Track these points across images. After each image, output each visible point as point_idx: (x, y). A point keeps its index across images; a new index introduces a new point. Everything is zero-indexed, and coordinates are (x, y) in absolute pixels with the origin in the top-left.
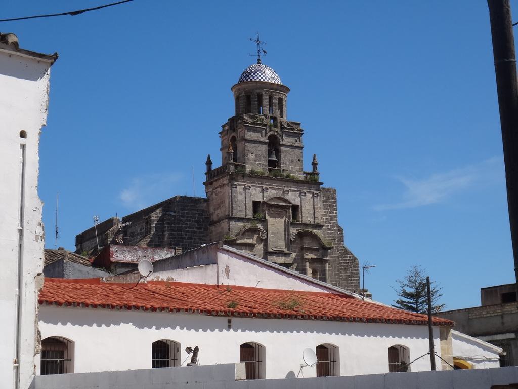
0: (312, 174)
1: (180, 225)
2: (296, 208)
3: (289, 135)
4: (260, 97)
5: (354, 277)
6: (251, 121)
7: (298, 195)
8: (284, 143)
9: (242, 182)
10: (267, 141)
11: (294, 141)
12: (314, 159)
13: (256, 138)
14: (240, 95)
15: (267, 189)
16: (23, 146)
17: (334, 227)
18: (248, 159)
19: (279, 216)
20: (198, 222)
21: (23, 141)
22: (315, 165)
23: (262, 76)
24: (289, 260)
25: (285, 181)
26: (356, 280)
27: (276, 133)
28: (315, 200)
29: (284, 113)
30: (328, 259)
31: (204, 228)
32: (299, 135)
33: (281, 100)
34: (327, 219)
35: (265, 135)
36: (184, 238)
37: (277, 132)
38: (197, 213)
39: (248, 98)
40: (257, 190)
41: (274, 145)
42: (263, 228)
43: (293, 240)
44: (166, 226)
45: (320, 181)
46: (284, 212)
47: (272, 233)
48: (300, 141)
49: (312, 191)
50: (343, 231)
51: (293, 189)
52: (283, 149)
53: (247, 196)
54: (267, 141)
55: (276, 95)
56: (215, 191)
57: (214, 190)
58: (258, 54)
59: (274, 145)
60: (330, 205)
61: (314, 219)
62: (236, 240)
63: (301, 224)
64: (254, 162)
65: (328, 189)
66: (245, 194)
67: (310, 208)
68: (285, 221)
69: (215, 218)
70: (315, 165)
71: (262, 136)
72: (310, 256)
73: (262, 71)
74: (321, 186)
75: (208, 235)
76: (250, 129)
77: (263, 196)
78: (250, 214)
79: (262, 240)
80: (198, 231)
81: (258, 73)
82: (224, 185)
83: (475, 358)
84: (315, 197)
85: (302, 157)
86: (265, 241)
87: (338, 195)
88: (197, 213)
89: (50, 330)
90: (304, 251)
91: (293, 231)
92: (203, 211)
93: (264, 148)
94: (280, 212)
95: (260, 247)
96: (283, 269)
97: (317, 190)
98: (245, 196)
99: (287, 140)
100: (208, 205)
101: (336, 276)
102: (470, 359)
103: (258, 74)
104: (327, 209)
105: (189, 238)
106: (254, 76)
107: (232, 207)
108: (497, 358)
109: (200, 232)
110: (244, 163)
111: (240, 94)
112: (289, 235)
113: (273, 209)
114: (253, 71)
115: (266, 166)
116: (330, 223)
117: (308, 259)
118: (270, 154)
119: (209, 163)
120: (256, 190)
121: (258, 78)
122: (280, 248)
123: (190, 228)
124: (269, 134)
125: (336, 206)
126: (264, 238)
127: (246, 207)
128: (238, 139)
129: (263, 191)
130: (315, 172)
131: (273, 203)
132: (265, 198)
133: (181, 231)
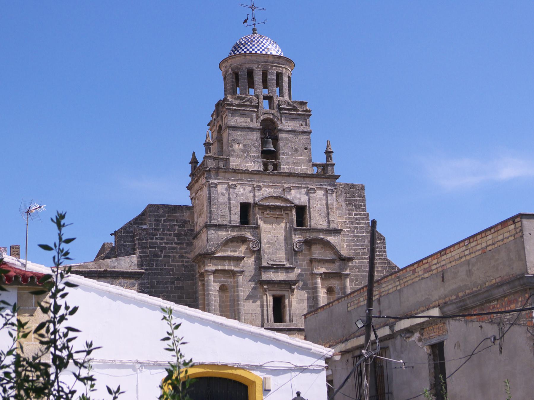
0: (325, 167)
1: (154, 241)
2: (302, 211)
3: (291, 118)
4: (250, 74)
6: (236, 102)
7: (304, 192)
8: (284, 128)
9: (225, 180)
10: (259, 126)
11: (298, 125)
12: (328, 146)
13: (244, 124)
15: (259, 187)
17: (363, 232)
18: (233, 151)
19: (277, 220)
20: (178, 235)
22: (328, 153)
23: (253, 48)
24: (292, 276)
25: (284, 176)
27: (271, 117)
28: (329, 198)
29: (284, 91)
30: (348, 272)
32: (306, 116)
33: (279, 76)
34: (352, 223)
35: (257, 119)
36: (160, 256)
37: (273, 114)
38: (176, 225)
40: (246, 190)
41: (269, 131)
42: (253, 236)
43: (296, 249)
44: (137, 242)
45: (336, 173)
46: (285, 215)
48: (306, 125)
49: (324, 187)
50: (384, 239)
51: (297, 185)
52: (282, 135)
53: (231, 197)
54: (259, 126)
55: (272, 69)
57: (196, 194)
58: (253, 23)
59: (269, 131)
60: (355, 205)
61: (329, 222)
62: (214, 253)
63: (308, 229)
64: (241, 153)
65: (352, 185)
66: (229, 195)
67: (323, 208)
68: (286, 227)
70: (328, 153)
71: (252, 121)
72: (322, 270)
73: (254, 41)
74: (338, 181)
75: (191, 251)
76: (234, 113)
77: (254, 196)
78: (236, 218)
79: (253, 252)
80: (179, 246)
83: (268, 366)
84: (329, 195)
85: (310, 144)
86: (258, 253)
87: (366, 192)
88: (176, 225)
90: (314, 264)
91: (297, 238)
92: (185, 222)
93: (255, 136)
94: (278, 215)
95: (250, 261)
97: (330, 186)
98: (228, 197)
99: (287, 124)
102: (260, 368)
103: (249, 45)
104: (352, 210)
105: (165, 256)
106: (244, 48)
107: (210, 212)
108: (320, 366)
109: (181, 248)
110: (229, 156)
111: (226, 72)
112: (292, 244)
113: (268, 212)
114: (243, 42)
115: (258, 158)
116: (356, 228)
117: (321, 275)
118: (264, 142)
120: (244, 189)
122: (279, 262)
124: (262, 118)
125: (365, 206)
126: (255, 249)
127: (230, 211)
128: (223, 127)
129: (254, 189)
130: (328, 163)
131: (268, 204)
132: (256, 199)
133: (154, 247)
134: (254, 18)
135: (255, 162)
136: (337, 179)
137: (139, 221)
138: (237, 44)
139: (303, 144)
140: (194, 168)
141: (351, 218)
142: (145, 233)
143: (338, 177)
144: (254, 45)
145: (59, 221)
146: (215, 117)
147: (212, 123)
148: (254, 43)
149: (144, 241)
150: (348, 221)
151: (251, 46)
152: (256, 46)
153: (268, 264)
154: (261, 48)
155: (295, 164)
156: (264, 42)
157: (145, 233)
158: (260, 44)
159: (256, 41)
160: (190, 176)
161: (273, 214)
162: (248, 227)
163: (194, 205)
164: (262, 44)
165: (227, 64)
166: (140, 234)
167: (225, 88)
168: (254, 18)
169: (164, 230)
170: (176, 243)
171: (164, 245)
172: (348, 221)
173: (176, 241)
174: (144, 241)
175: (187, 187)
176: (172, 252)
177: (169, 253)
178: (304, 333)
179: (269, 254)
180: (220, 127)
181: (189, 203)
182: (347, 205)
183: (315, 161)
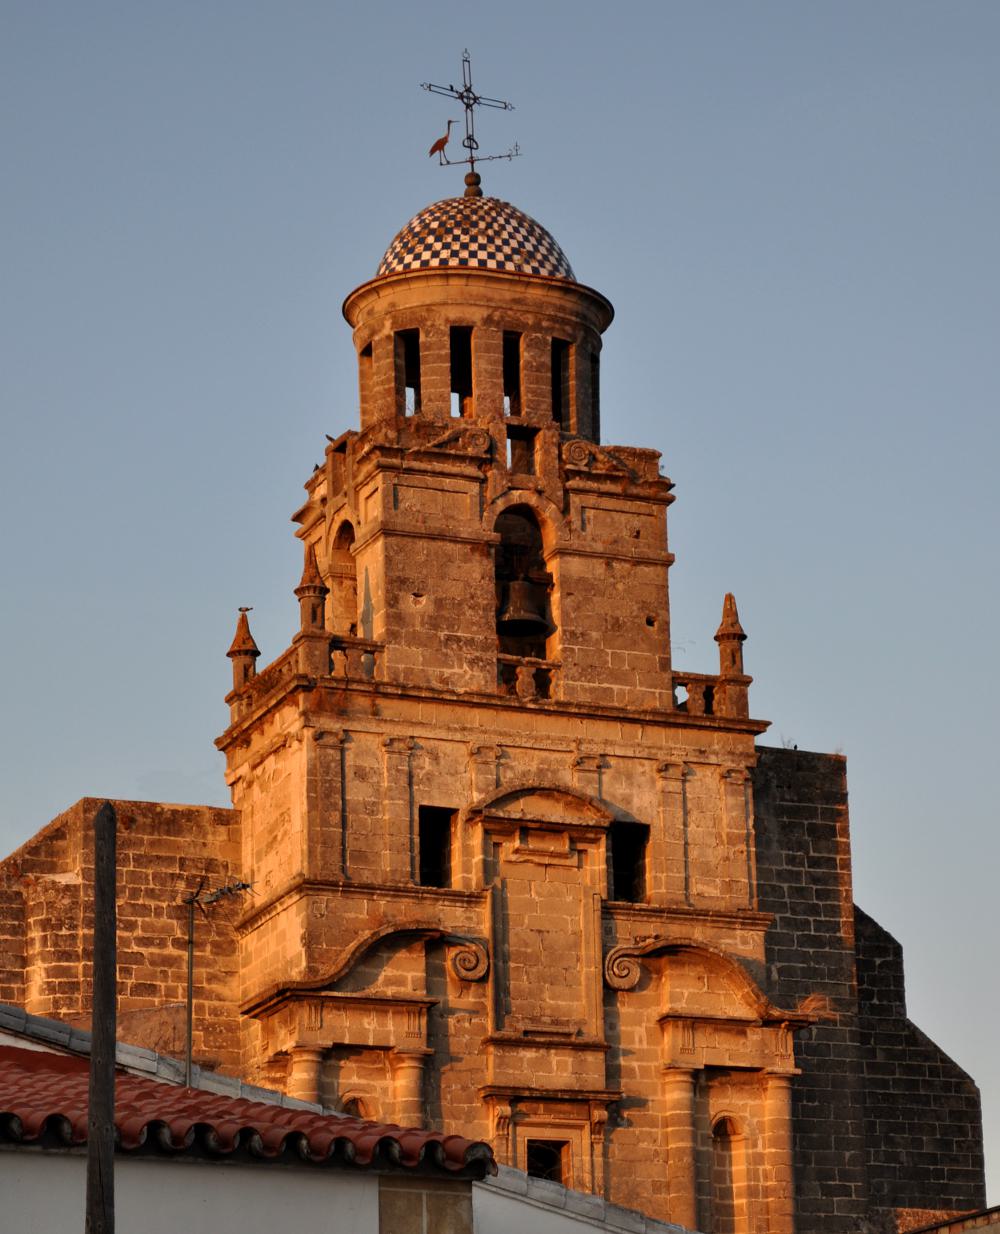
2: (628, 842)
5: (955, 1160)
14: (377, 338)
22: (732, 637)
23: (474, 247)
25: (575, 715)
26: (967, 1175)
31: (215, 945)
34: (799, 892)
38: (180, 877)
45: (754, 714)
56: (259, 771)
70: (732, 637)
73: (475, 225)
81: (457, 232)
88: (180, 877)
92: (210, 865)
93: (478, 573)
100: (234, 840)
101: (847, 1154)
103: (456, 238)
111: (373, 333)
114: (435, 225)
115: (485, 648)
119: (245, 650)
121: (473, 254)
123: (145, 942)
134: (470, 138)
135: (473, 663)
136: (758, 733)
137: (43, 858)
138: (411, 230)
139: (644, 605)
140: (246, 672)
141: (799, 873)
142: (66, 901)
143: (761, 727)
144: (474, 239)
145: (532, 930)
146: (322, 490)
147: (311, 517)
148: (474, 231)
149: (64, 932)
150: (785, 886)
151: (465, 239)
152: (482, 240)
153: (516, 1030)
154: (499, 249)
155: (617, 677)
156: (509, 228)
157: (66, 901)
158: (498, 233)
159: (482, 225)
160: (229, 700)
161: (533, 852)
162: (446, 894)
163: (246, 807)
164: (505, 235)
165: (380, 303)
166: (50, 905)
167: (363, 388)
168: (470, 138)
169: (135, 893)
170: (177, 943)
171: (136, 949)
172: (785, 886)
173: (179, 934)
174: (64, 932)
175: (218, 742)
176: (164, 973)
177: (153, 976)
178: (84, 1151)
180: (346, 530)
181: (225, 802)
182: (784, 827)
183: (680, 664)
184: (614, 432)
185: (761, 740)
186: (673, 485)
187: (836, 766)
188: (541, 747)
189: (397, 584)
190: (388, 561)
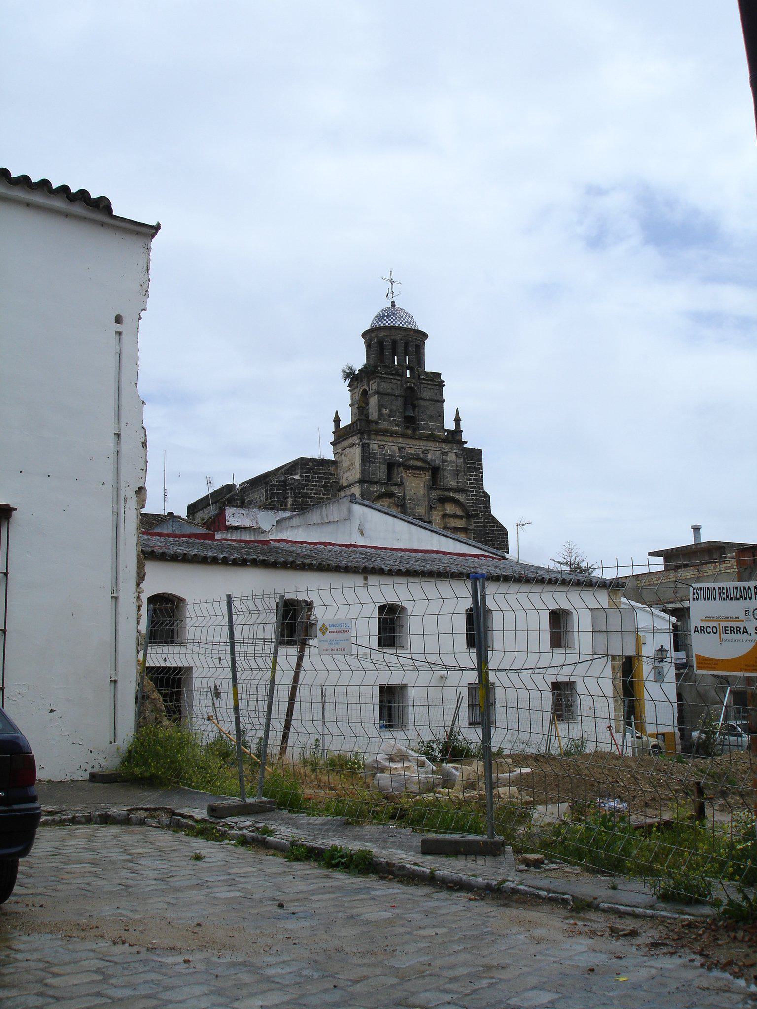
2: (435, 471)
4: (406, 345)
16: (119, 333)
21: (118, 327)
22: (458, 420)
39: (381, 344)
47: (410, 499)
69: (344, 483)
70: (458, 420)
74: (465, 446)
82: (353, 445)
89: (151, 588)
91: (434, 495)
92: (331, 474)
93: (399, 402)
96: (424, 522)
116: (475, 488)
119: (337, 420)
132: (397, 392)
179: (410, 509)
184: (428, 368)
185: (465, 446)
186: (157, 228)
187: (480, 452)
188: (413, 447)
189: (380, 406)
190: (379, 400)
